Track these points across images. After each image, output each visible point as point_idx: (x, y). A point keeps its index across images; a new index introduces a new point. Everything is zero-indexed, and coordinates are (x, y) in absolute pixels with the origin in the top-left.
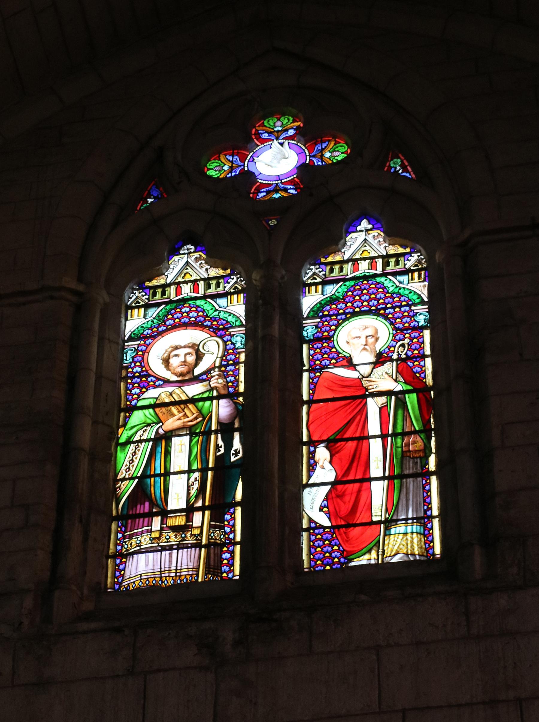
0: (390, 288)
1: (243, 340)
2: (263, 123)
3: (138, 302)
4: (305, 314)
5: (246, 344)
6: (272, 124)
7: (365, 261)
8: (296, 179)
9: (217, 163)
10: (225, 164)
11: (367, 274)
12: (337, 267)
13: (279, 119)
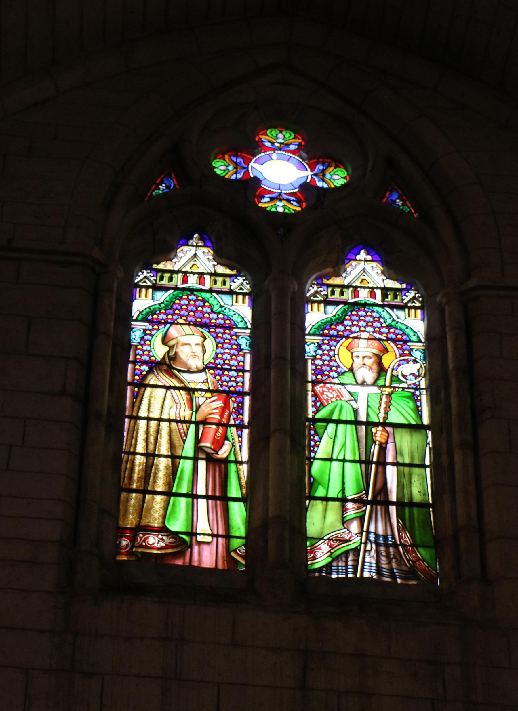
0: (214, 306)
1: (248, 342)
2: (266, 132)
3: (145, 282)
4: (135, 314)
5: (251, 346)
6: (275, 135)
7: (194, 275)
8: (298, 194)
9: (222, 162)
10: (229, 165)
11: (195, 288)
12: (167, 276)
13: (281, 132)
